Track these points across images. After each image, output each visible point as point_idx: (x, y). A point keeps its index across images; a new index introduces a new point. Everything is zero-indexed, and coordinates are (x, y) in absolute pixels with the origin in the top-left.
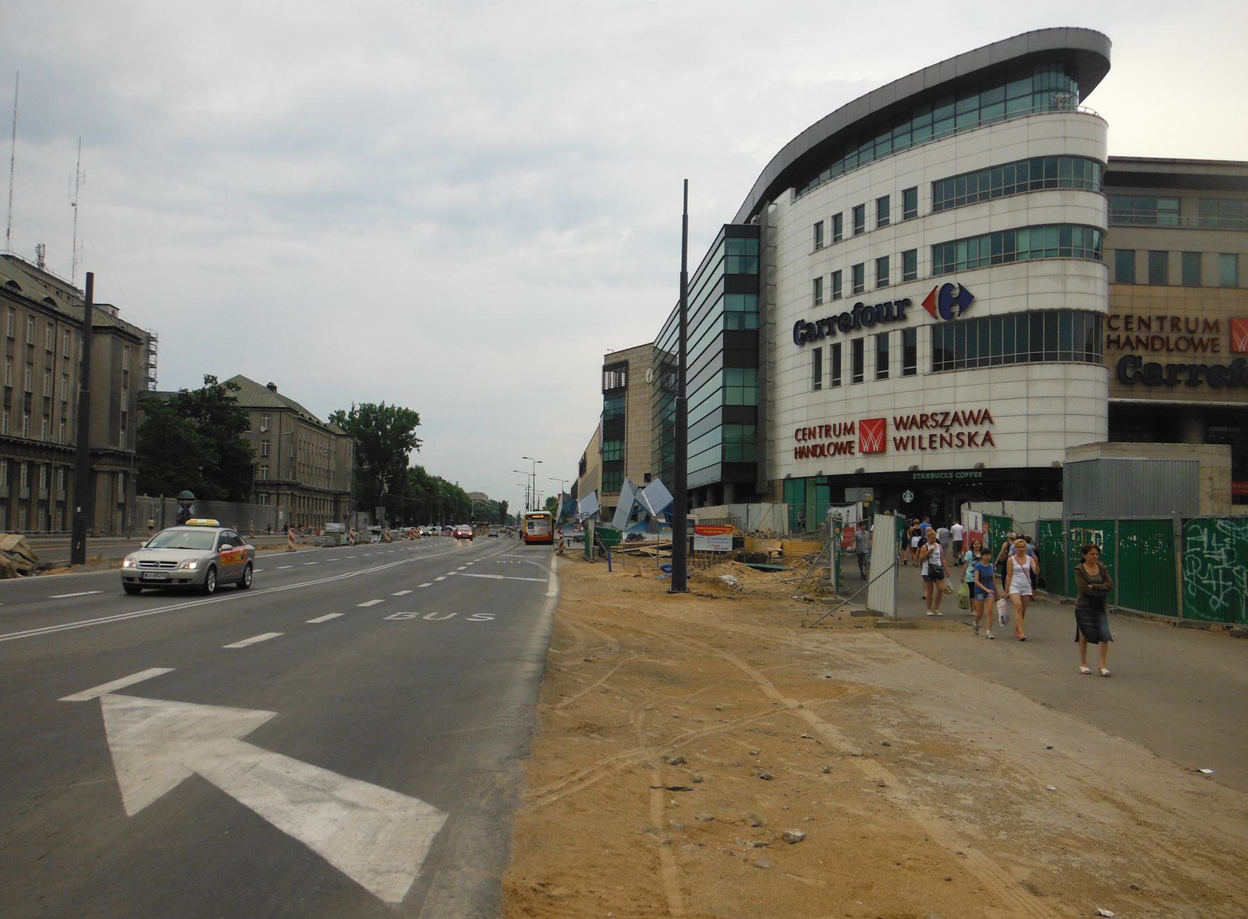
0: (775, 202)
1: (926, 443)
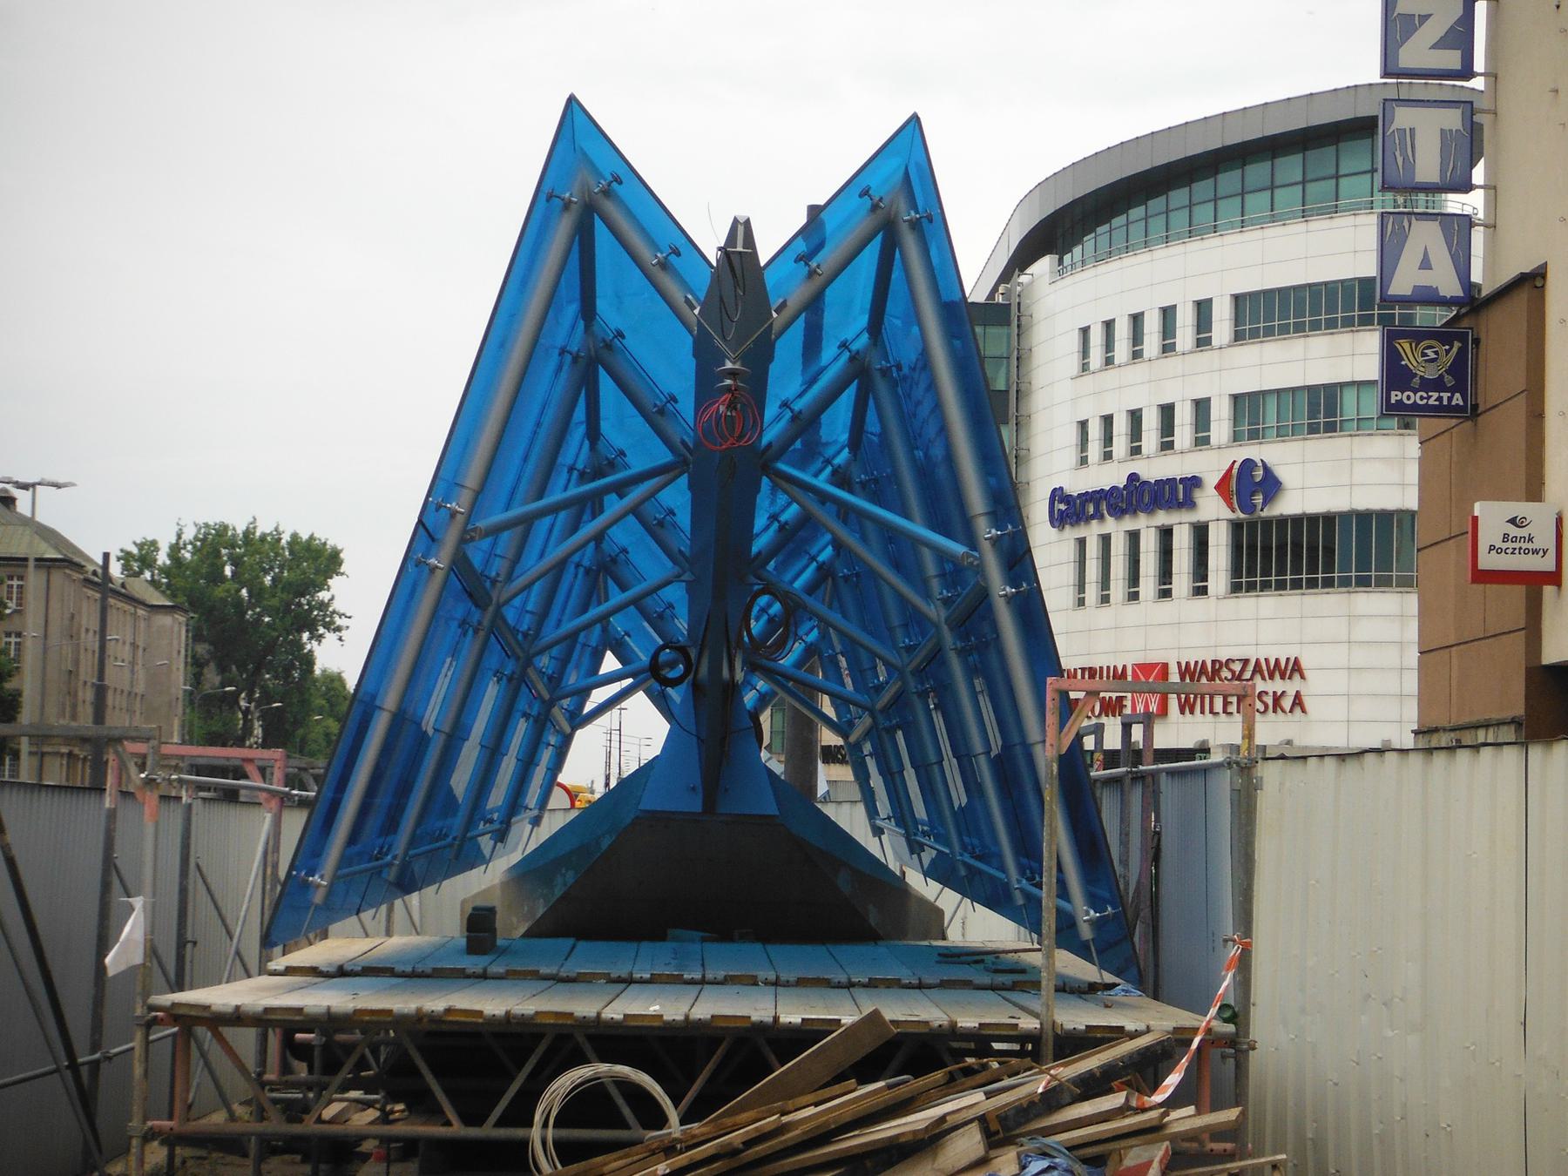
0: (1028, 271)
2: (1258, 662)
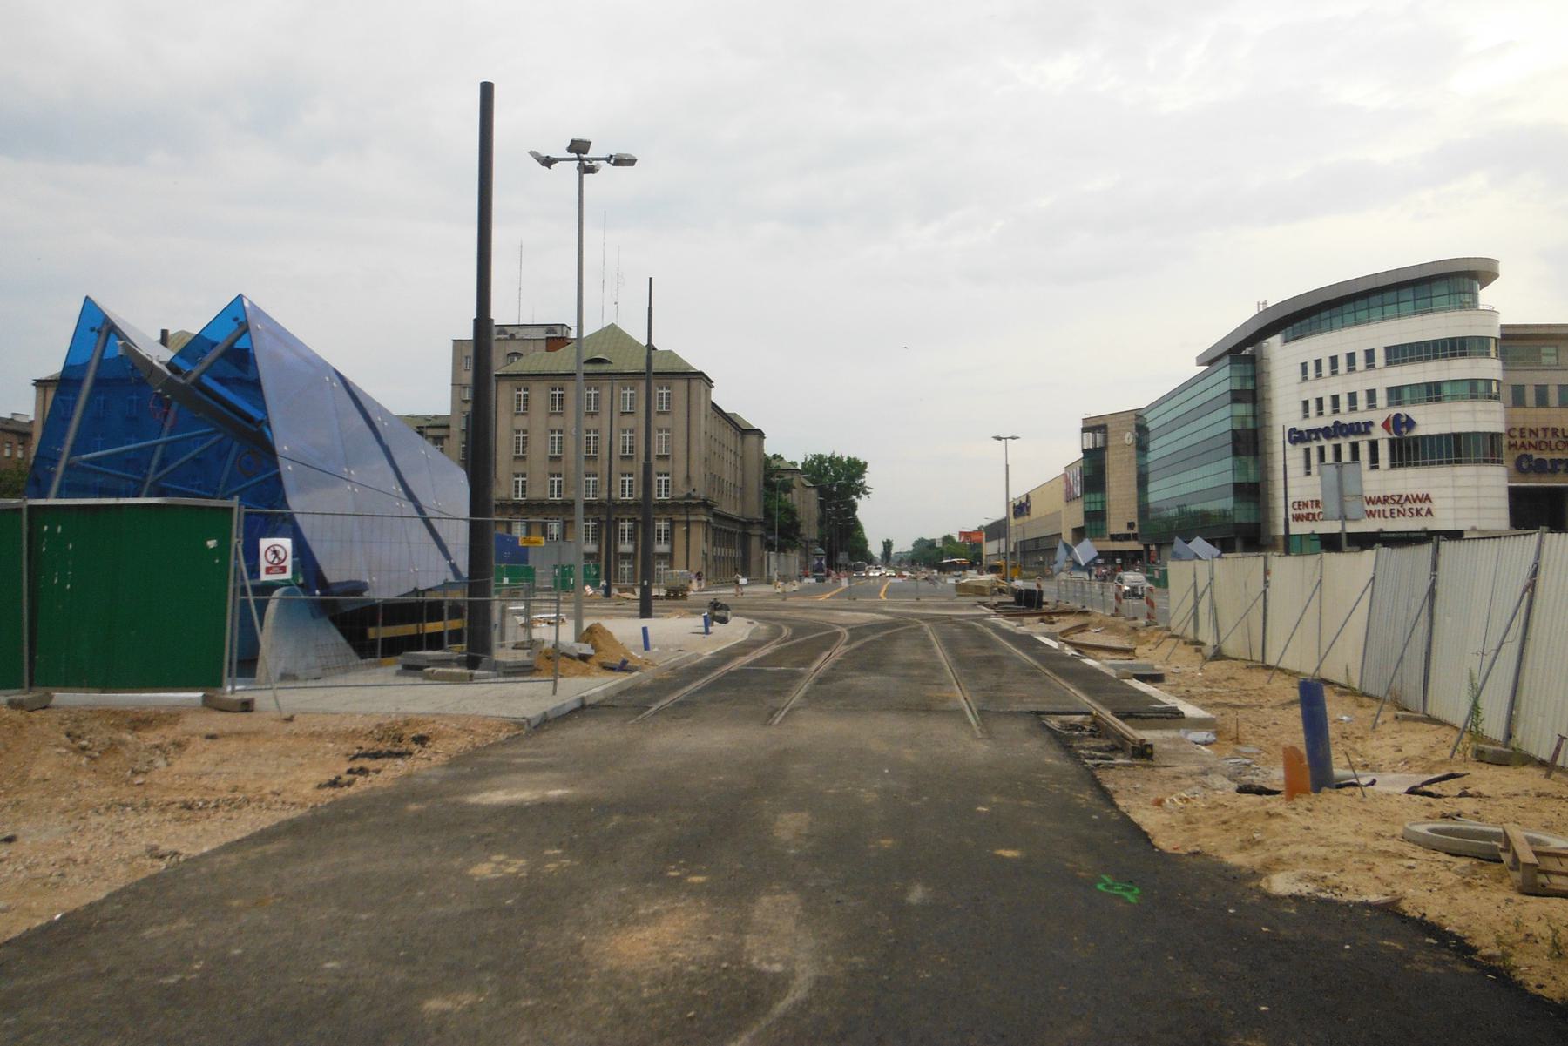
1: (1388, 514)
2: (1407, 497)
